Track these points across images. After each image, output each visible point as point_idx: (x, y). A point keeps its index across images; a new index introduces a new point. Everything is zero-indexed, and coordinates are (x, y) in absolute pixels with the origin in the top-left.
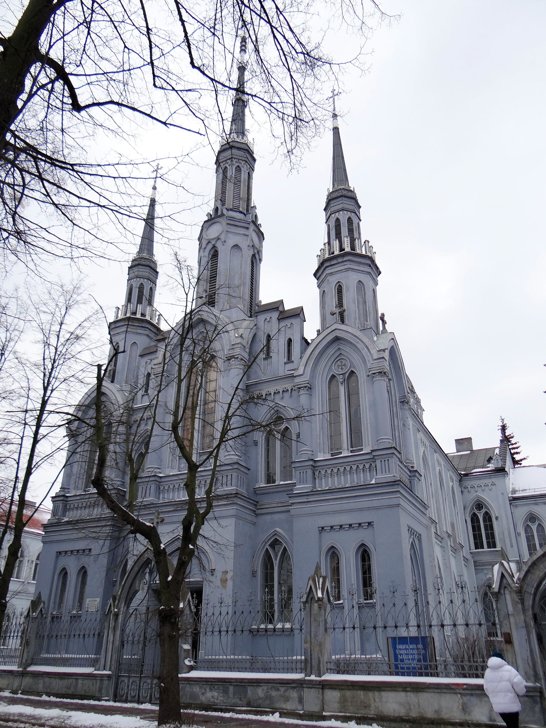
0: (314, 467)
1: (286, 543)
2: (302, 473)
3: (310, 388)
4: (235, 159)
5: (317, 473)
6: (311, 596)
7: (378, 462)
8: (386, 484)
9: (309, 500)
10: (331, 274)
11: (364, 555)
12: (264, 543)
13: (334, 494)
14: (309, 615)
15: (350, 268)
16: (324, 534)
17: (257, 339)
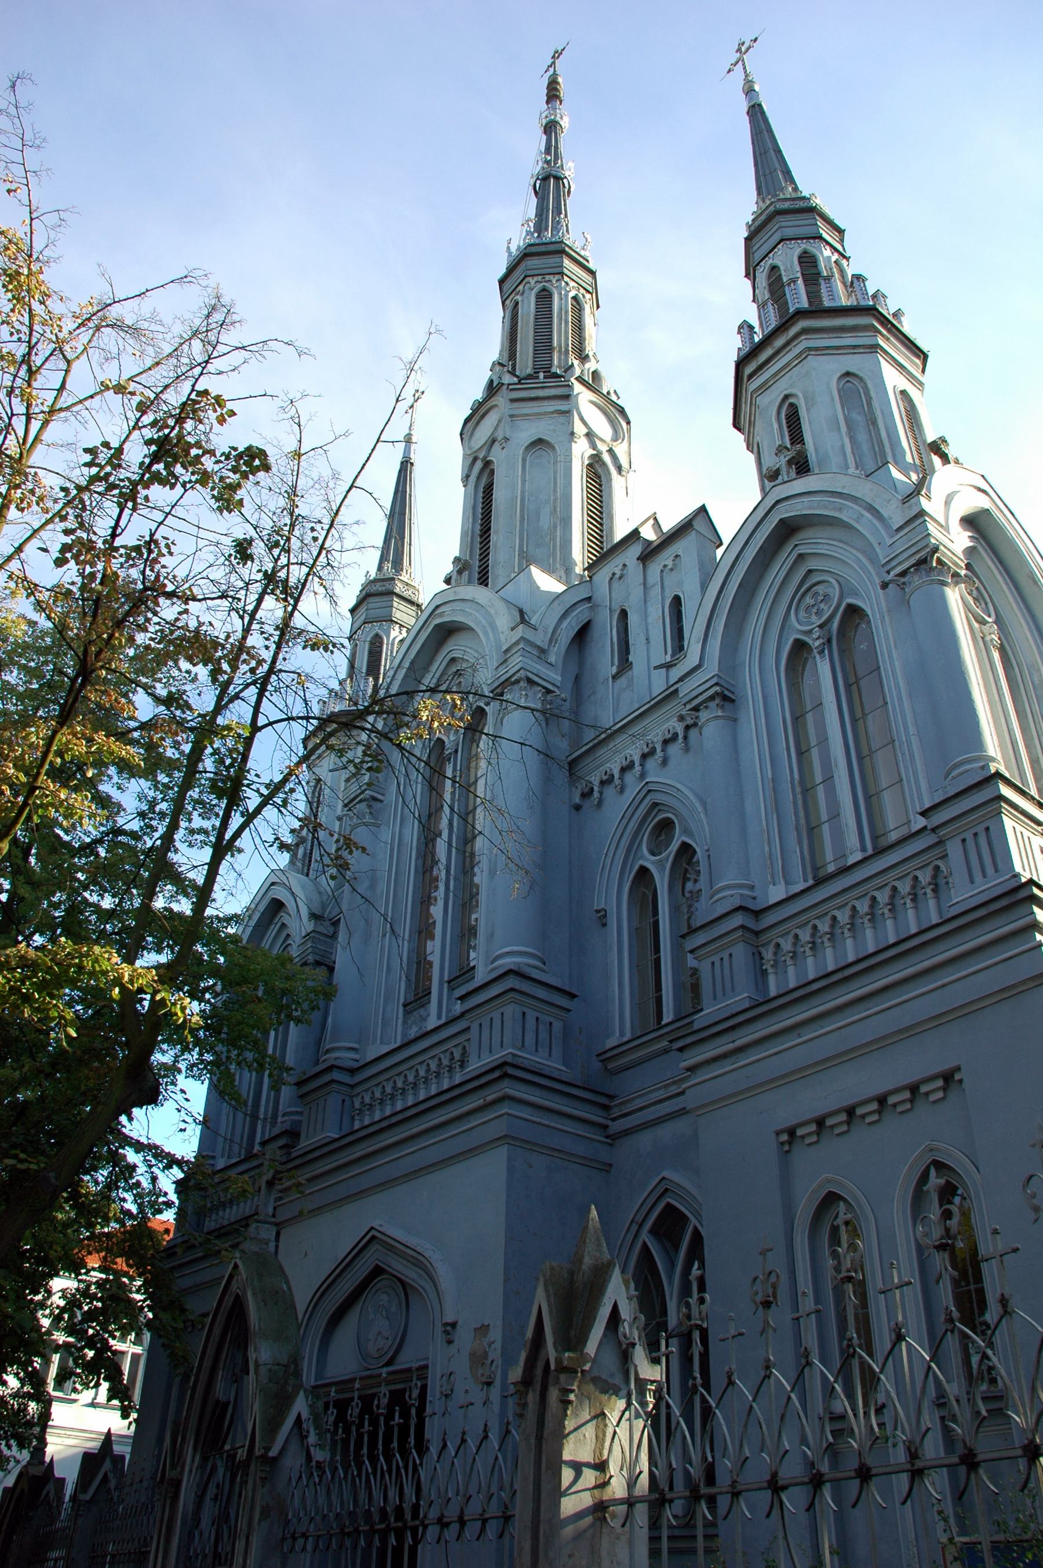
0: (757, 934)
3: (725, 697)
4: (539, 277)
5: (768, 954)
7: (954, 848)
9: (738, 1044)
10: (764, 387)
12: (635, 1227)
13: (815, 1001)
15: (810, 349)
16: (803, 1157)
17: (596, 632)
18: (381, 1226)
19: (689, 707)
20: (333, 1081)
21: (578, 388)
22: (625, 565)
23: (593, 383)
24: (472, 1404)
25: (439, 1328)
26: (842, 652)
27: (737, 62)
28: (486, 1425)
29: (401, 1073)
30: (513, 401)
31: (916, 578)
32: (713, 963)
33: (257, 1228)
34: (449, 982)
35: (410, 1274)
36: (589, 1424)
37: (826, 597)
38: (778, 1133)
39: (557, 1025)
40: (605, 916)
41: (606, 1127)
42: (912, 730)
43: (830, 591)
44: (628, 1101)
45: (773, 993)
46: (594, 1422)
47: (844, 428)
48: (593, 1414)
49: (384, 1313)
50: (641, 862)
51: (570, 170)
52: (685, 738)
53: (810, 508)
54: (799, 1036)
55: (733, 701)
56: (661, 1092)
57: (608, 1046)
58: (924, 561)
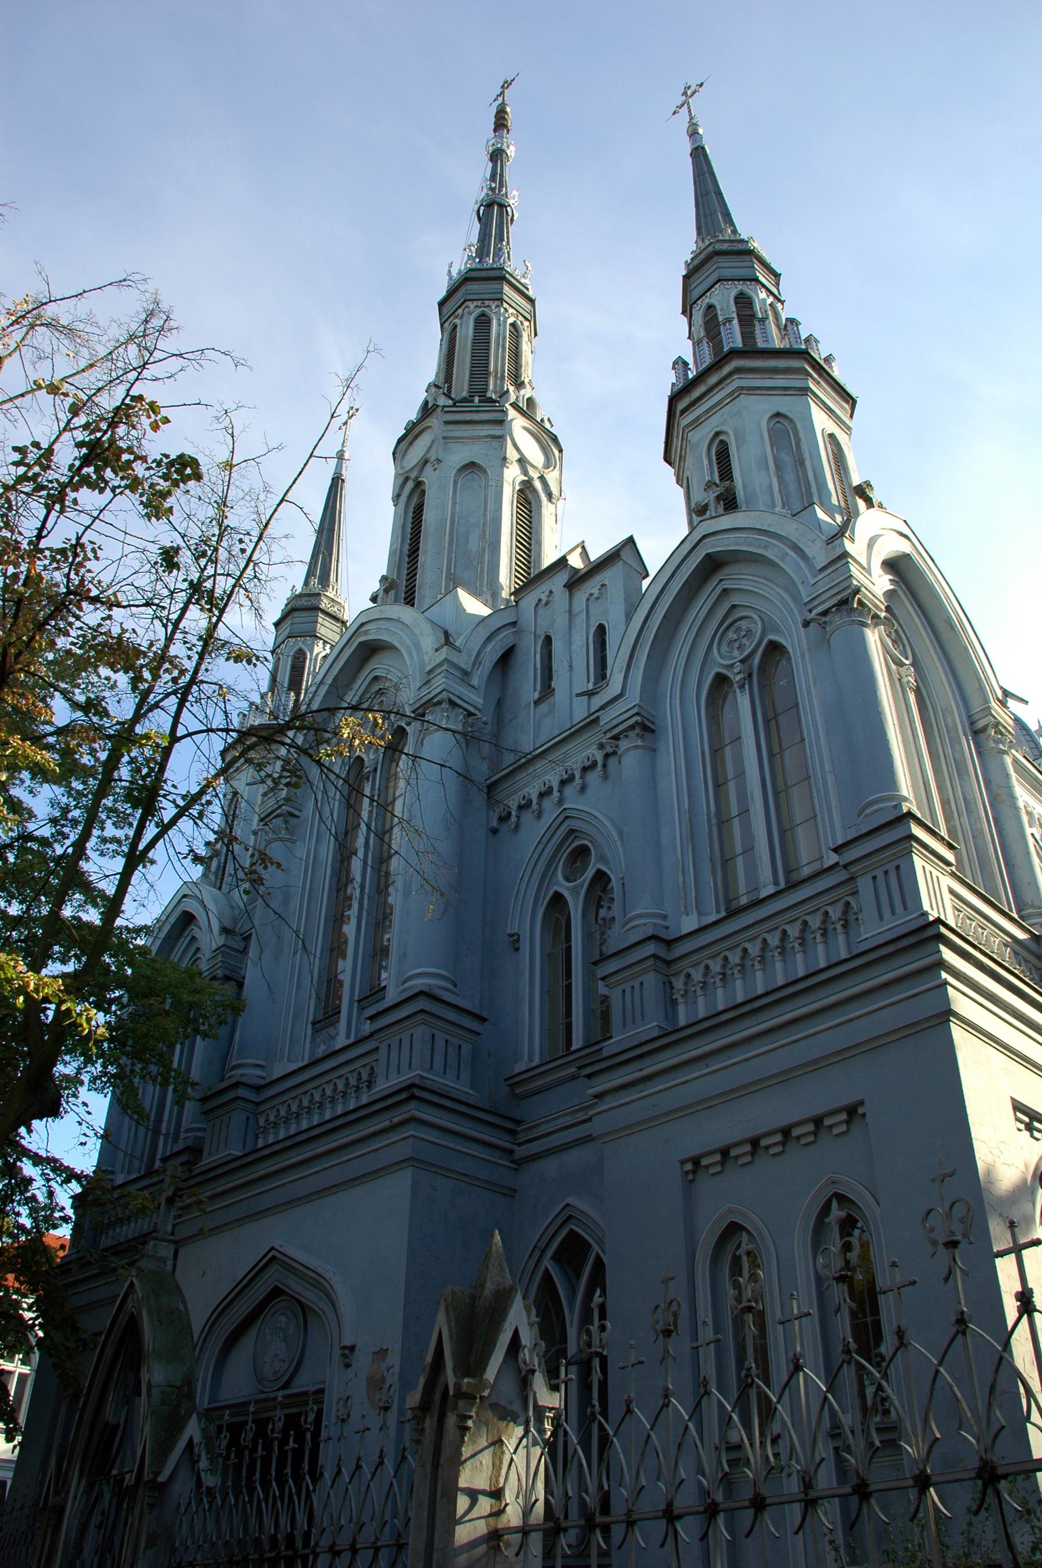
0: (669, 963)
3: (646, 727)
4: (478, 300)
5: (679, 983)
7: (864, 884)
8: (891, 948)
9: (645, 1072)
10: (696, 423)
11: (840, 1218)
12: (537, 1254)
15: (742, 388)
17: (519, 657)
18: (281, 1246)
19: (609, 735)
20: (238, 1098)
21: (512, 413)
22: (551, 592)
23: (528, 409)
24: (369, 1429)
25: (337, 1352)
27: (682, 105)
28: (382, 1451)
30: (447, 423)
31: (837, 618)
32: (624, 991)
33: (155, 1246)
34: (359, 1001)
35: (309, 1295)
36: (487, 1451)
37: (749, 631)
38: (683, 1162)
39: (466, 1048)
40: (518, 940)
41: (512, 1152)
42: (827, 767)
44: (534, 1126)
46: (492, 1449)
48: (490, 1441)
49: (281, 1335)
50: (556, 888)
51: (514, 198)
52: (604, 766)
54: (707, 1066)
55: (653, 731)
56: (568, 1118)
57: (517, 1071)
58: (845, 602)
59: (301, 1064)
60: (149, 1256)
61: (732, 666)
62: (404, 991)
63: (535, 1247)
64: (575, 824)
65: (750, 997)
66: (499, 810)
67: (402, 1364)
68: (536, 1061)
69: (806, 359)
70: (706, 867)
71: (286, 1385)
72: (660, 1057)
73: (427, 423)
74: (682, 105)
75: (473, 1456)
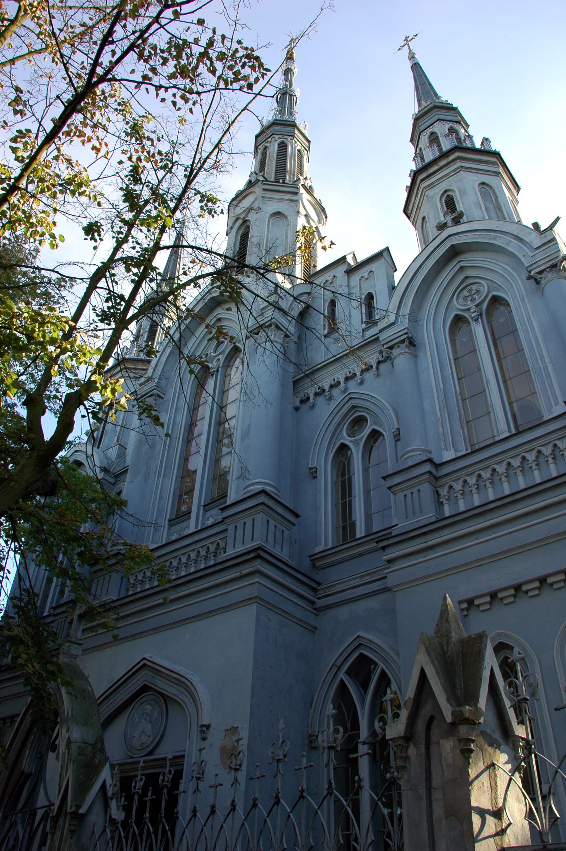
0: (437, 479)
1: (385, 660)
2: (409, 496)
3: (412, 342)
5: (444, 492)
6: (425, 712)
9: (429, 543)
10: (431, 186)
12: (335, 669)
13: (490, 516)
14: (422, 790)
15: (462, 167)
18: (151, 657)
19: (385, 346)
21: (302, 190)
22: (334, 276)
23: (309, 190)
24: (221, 785)
25: (195, 730)
26: (489, 322)
27: (404, 45)
28: (233, 801)
29: (168, 560)
30: (265, 190)
31: (550, 275)
32: (405, 496)
33: (69, 647)
34: (204, 506)
35: (171, 690)
36: (485, 773)
37: (478, 291)
38: (460, 603)
39: (286, 533)
40: (316, 472)
41: (314, 603)
42: (547, 360)
43: (481, 289)
44: (330, 586)
45: (447, 514)
46: (488, 772)
47: (484, 209)
48: (486, 765)
49: (147, 718)
50: (342, 441)
51: (297, 91)
52: (377, 368)
53: (473, 239)
54: (477, 539)
55: (414, 346)
56: (358, 580)
57: (316, 551)
58: (554, 266)
59: (160, 544)
60: (64, 653)
61: (468, 310)
62: (246, 492)
63: (333, 665)
64: (357, 402)
65: (514, 491)
66: (301, 396)
67: (249, 738)
68: (330, 546)
69: (497, 158)
70: (457, 424)
71: (151, 753)
72: (440, 533)
73: (252, 189)
74: (404, 45)
75: (477, 777)
